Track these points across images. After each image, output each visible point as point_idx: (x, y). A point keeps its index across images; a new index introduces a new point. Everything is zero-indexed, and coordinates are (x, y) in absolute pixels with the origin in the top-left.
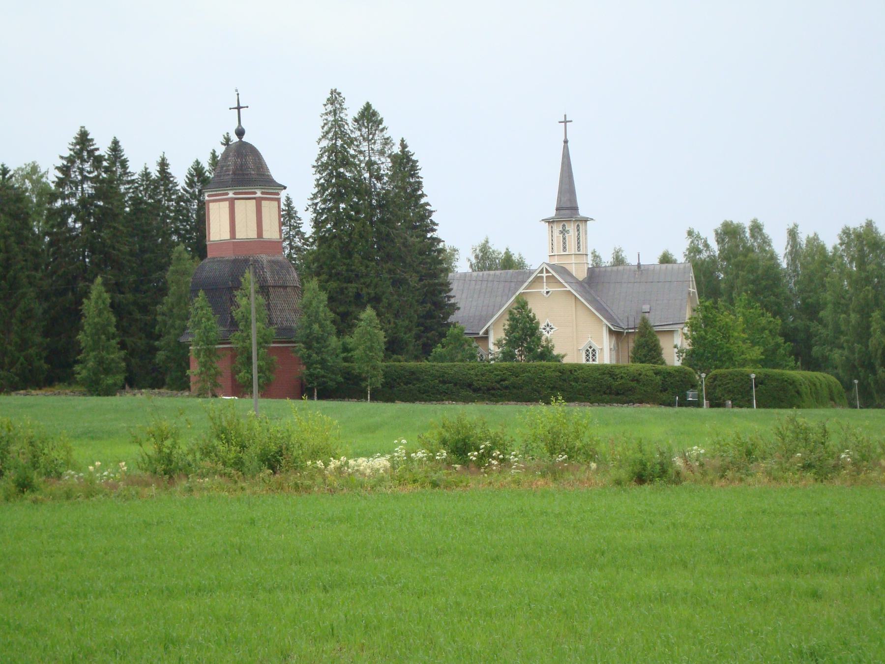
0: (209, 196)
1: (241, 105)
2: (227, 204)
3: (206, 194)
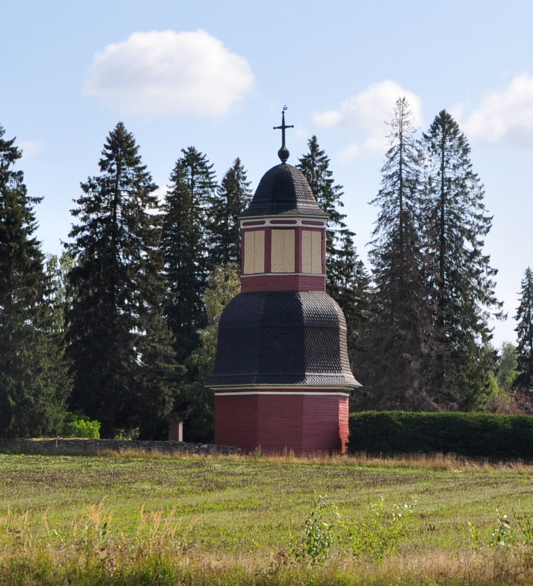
0: (244, 224)
1: (281, 125)
2: (263, 232)
3: (242, 222)
